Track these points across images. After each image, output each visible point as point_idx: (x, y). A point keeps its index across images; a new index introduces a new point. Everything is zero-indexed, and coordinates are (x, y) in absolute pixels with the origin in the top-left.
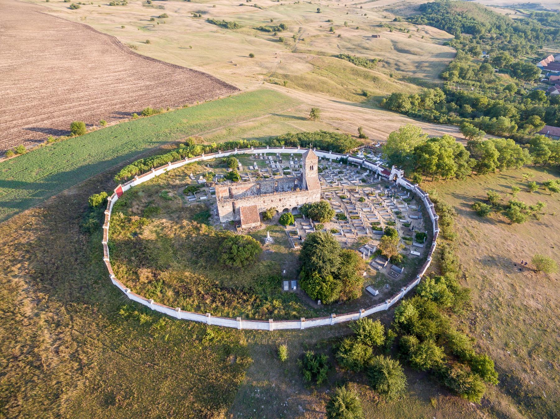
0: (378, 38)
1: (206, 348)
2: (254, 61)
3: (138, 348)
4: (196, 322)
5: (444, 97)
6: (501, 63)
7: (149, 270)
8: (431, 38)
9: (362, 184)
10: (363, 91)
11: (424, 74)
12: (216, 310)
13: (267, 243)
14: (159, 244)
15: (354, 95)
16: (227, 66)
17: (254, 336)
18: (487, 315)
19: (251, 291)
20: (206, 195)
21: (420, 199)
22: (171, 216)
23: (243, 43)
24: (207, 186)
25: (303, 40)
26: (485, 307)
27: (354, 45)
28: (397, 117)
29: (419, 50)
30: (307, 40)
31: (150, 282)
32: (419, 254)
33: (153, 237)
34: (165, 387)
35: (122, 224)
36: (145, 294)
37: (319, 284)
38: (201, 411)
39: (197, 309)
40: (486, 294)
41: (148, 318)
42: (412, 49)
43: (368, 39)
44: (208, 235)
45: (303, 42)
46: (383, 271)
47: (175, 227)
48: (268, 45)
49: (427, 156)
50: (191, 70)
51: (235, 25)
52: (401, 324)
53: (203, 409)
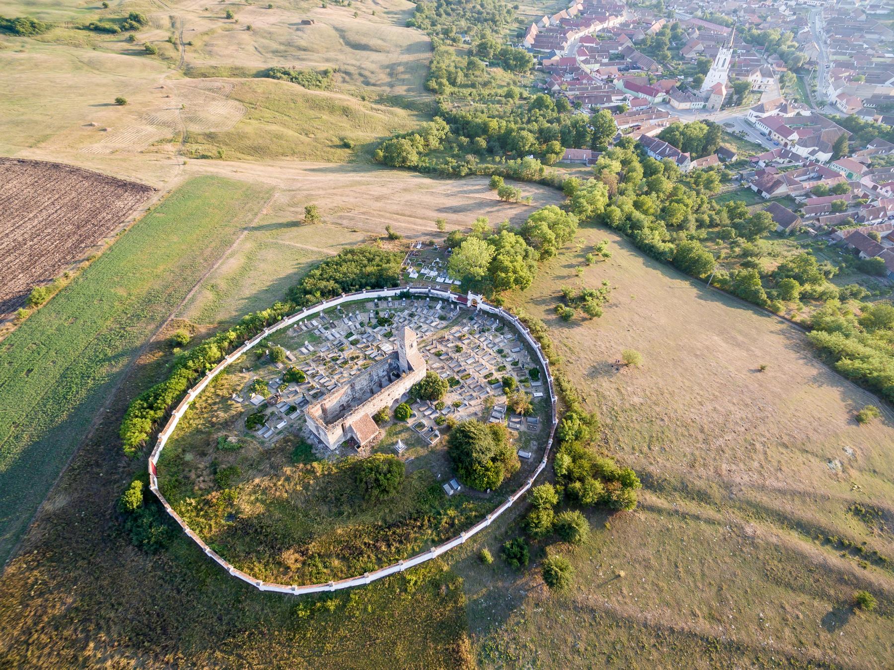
0: (313, 25)
1: (415, 594)
2: (130, 112)
3: (346, 637)
4: (389, 576)
5: (447, 127)
6: (488, 53)
7: (292, 551)
8: (385, 13)
9: (445, 323)
10: (342, 139)
11: (405, 88)
12: (398, 551)
13: (401, 451)
14: (277, 515)
15: (333, 150)
16: (90, 137)
17: (452, 556)
18: (612, 429)
19: (420, 514)
20: (281, 419)
21: (510, 323)
22: (260, 471)
23: (78, 68)
24: (272, 405)
25: (190, 44)
26: (608, 421)
27: (281, 44)
28: (405, 175)
29: (380, 42)
30: (198, 43)
31: (304, 563)
32: (541, 394)
33: (260, 509)
34: (400, 651)
35: (202, 513)
36: (310, 579)
37: (484, 475)
38: (447, 649)
39: (380, 564)
40: (604, 408)
41: (337, 602)
42: (373, 42)
43: (298, 30)
44: (329, 474)
45: (192, 48)
46: (523, 428)
47: (280, 483)
48: (131, 66)
49: (503, 275)
50: (22, 162)
51: (33, 25)
52: (564, 476)
53: (447, 646)
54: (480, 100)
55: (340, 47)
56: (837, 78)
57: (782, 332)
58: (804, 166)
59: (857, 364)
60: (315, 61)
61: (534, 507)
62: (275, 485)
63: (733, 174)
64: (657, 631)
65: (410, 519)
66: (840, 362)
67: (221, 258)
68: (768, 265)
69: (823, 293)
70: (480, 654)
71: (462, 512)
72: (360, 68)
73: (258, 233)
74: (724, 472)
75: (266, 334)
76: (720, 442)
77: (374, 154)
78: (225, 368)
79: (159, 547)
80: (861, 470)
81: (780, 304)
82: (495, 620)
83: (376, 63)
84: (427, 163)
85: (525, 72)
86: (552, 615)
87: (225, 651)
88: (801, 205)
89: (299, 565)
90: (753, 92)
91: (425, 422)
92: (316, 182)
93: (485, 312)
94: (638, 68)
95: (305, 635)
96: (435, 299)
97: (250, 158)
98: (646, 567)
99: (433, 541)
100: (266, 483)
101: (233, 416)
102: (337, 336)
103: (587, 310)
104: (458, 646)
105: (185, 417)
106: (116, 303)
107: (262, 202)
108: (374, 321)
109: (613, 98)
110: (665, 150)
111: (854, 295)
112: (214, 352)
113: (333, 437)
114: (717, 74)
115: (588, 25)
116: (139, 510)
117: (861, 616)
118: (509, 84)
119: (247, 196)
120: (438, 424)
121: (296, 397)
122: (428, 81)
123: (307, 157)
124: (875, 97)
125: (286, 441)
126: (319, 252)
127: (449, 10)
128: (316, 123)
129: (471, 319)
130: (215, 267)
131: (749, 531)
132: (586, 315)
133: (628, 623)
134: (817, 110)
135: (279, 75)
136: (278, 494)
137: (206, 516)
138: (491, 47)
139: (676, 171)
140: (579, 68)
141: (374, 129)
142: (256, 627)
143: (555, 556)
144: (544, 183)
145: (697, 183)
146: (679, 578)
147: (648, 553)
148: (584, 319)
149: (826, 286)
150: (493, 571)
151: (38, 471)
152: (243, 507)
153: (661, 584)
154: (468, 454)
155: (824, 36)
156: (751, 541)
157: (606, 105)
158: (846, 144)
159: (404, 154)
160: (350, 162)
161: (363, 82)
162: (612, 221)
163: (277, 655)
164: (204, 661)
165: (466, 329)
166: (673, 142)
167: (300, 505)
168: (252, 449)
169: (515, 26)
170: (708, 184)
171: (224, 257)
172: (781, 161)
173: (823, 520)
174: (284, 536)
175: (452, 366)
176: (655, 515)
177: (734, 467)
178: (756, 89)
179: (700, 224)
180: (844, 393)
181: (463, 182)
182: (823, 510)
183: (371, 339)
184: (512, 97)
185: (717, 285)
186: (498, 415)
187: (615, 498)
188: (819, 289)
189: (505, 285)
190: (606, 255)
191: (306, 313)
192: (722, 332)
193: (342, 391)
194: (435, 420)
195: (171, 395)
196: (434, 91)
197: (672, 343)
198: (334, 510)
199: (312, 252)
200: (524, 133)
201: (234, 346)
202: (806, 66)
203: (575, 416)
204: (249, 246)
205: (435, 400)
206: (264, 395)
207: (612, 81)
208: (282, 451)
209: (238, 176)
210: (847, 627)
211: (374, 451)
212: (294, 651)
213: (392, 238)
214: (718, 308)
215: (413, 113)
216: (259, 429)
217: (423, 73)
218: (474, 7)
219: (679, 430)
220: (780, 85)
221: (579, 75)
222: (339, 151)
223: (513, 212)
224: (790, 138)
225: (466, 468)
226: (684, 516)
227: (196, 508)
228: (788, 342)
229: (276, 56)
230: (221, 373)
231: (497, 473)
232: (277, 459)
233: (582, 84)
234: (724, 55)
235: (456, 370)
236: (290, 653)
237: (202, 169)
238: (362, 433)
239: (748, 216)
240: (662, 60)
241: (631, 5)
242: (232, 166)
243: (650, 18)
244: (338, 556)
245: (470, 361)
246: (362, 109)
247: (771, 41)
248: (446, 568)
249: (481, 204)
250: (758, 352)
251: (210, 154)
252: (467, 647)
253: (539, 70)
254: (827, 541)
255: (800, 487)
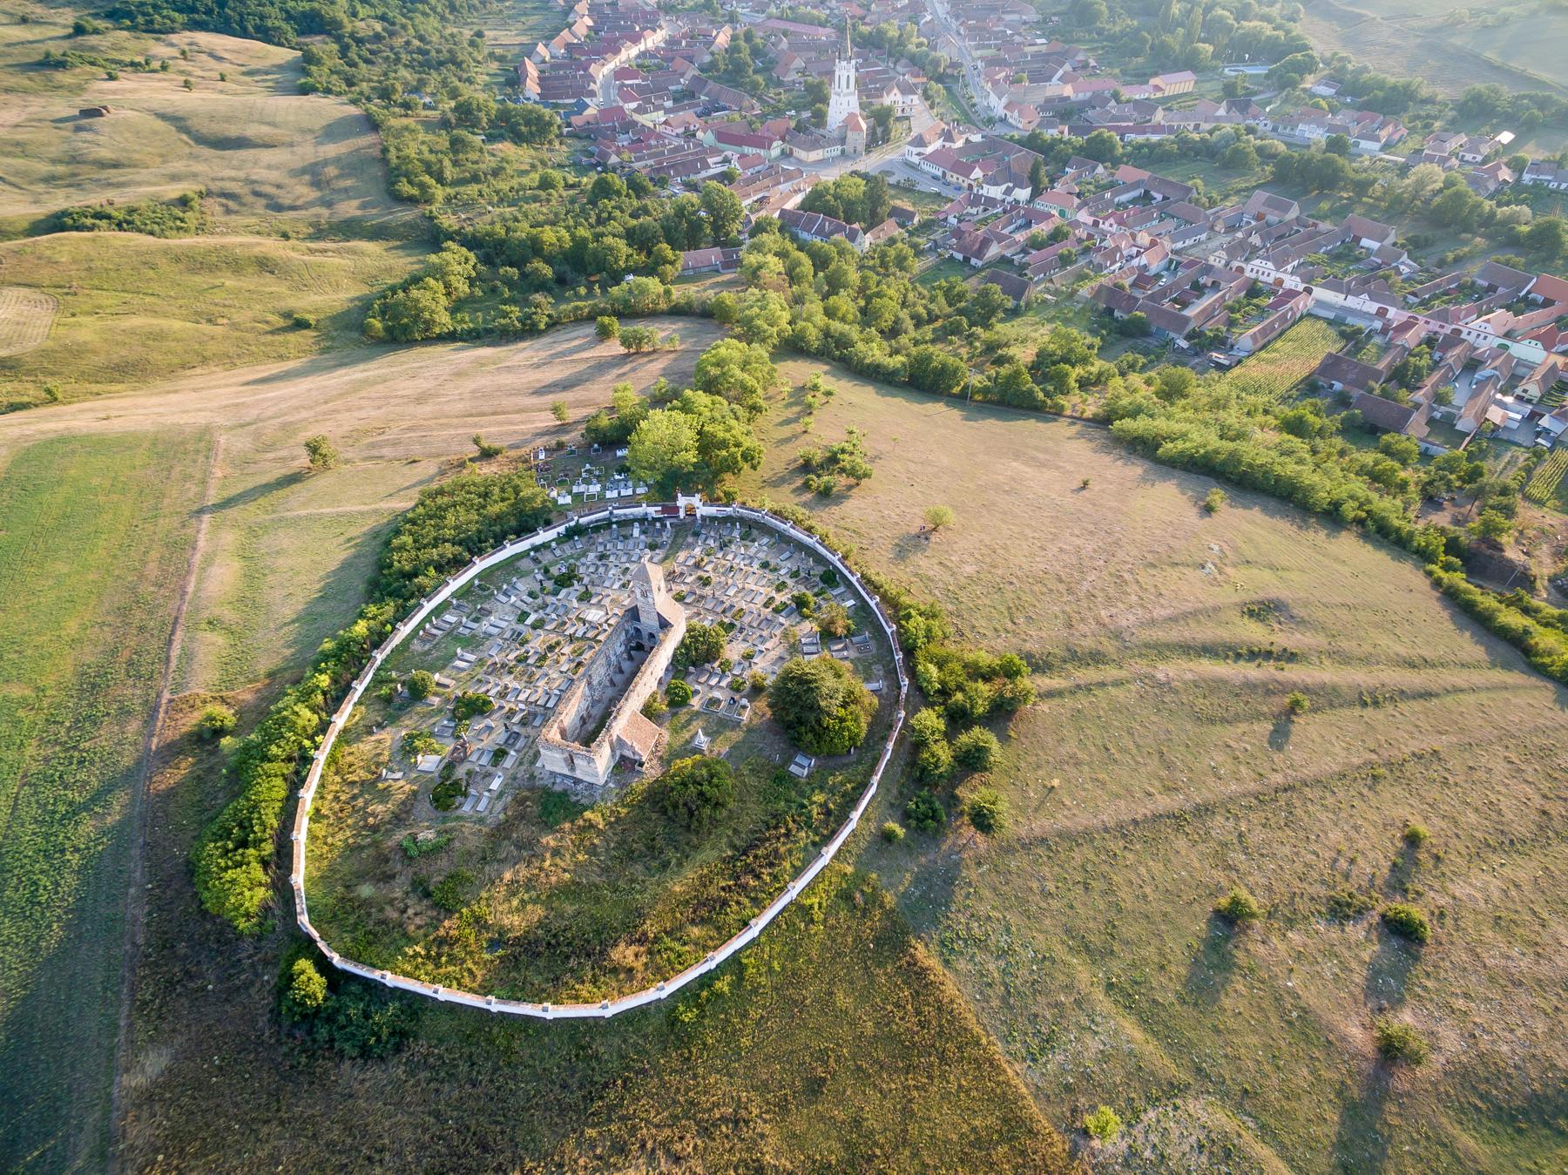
0: (108, 118)
1: (825, 920)
4: (780, 913)
5: (471, 255)
6: (479, 120)
7: (622, 946)
10: (287, 315)
11: (355, 203)
12: (775, 878)
13: (705, 747)
21: (756, 522)
24: (462, 760)
27: (54, 161)
29: (265, 129)
31: (650, 952)
32: (852, 602)
33: (537, 912)
35: (444, 959)
39: (759, 905)
43: (78, 129)
44: (618, 819)
49: (724, 453)
52: (938, 691)
54: (501, 200)
55: (187, 150)
56: (995, 83)
57: (1080, 435)
58: (1005, 212)
59: (1180, 445)
60: (150, 184)
61: (920, 745)
62: (541, 869)
63: (923, 242)
64: (1120, 831)
65: (768, 829)
66: (1160, 451)
67: (188, 572)
68: (1024, 355)
69: (1100, 374)
70: (942, 954)
71: (832, 791)
72: (249, 181)
73: (231, 513)
74: (1107, 620)
75: (378, 662)
76: (1086, 586)
77: (363, 329)
78: (339, 736)
79: (401, 1037)
80: (1235, 565)
81: (1061, 400)
82: (940, 905)
83: (278, 168)
84: (467, 322)
85: (550, 142)
86: (1001, 868)
87: (598, 1124)
88: (1024, 266)
89: (644, 959)
90: (898, 119)
91: (717, 694)
92: (283, 399)
93: (713, 519)
94: (724, 109)
95: (704, 1044)
96: (626, 523)
97: (119, 387)
98: (1076, 764)
99: (814, 844)
100: (524, 872)
101: (403, 803)
102: (503, 624)
103: (851, 472)
104: (912, 956)
105: (313, 838)
106: (21, 713)
107: (201, 459)
108: (549, 585)
109: (710, 161)
110: (822, 226)
111: (1132, 367)
112: (307, 718)
113: (599, 765)
114: (844, 100)
115: (617, 51)
116: (329, 1003)
117: (1300, 723)
118: (533, 166)
119: (160, 455)
120: (737, 690)
121: (493, 736)
122: (394, 183)
123: (238, 362)
124: (1048, 100)
125: (521, 802)
126: (376, 511)
127: (365, 53)
128: (218, 297)
129: (697, 535)
130: (191, 589)
131: (1160, 676)
132: (852, 481)
133: (1087, 836)
134: (987, 131)
135: (89, 221)
136: (554, 879)
137: (452, 960)
138: (480, 110)
139: (853, 254)
140: (634, 123)
141: (337, 287)
142: (628, 1068)
143: (971, 794)
144: (678, 312)
145: (884, 264)
146: (1115, 761)
147: (1071, 747)
148: (850, 488)
149: (1097, 366)
150: (907, 847)
151: (65, 1038)
152: (506, 922)
153: (1100, 776)
154: (814, 708)
155: (954, 24)
156: (1166, 686)
157: (704, 174)
158: (1043, 170)
159: (427, 315)
160: (324, 351)
161: (267, 207)
162: (808, 343)
163: (678, 1089)
164: (572, 1152)
165: (697, 551)
166: (830, 212)
167: (597, 880)
168: (471, 837)
169: (494, 66)
170: (901, 262)
171: (196, 570)
172: (974, 211)
173: (1223, 634)
174: (598, 933)
175: (709, 606)
176: (1057, 701)
177: (1114, 611)
178: (899, 114)
179: (919, 322)
180: (1179, 485)
181: (546, 340)
182: (1220, 623)
183: (561, 611)
184: (553, 187)
185: (978, 397)
186: (813, 649)
187: (1009, 695)
188: (1094, 369)
189: (731, 467)
190: (829, 393)
191: (428, 606)
192: (1017, 456)
193: (579, 693)
194: (730, 686)
195: (269, 811)
196: (412, 201)
197: (972, 486)
198: (655, 864)
199: (362, 513)
200: (609, 240)
201: (335, 700)
202: (949, 71)
203: (913, 613)
204: (229, 538)
205: (715, 659)
206: (437, 752)
207: (694, 135)
208: (523, 818)
209: (116, 426)
210: (1293, 738)
211: (666, 762)
212: (701, 1071)
213: (487, 454)
214: (993, 426)
215: (391, 244)
216: (461, 805)
217: (377, 171)
218: (408, 43)
219: (1035, 588)
220: (928, 103)
221: (642, 138)
222: (294, 338)
223: (658, 365)
224: (973, 176)
225: (812, 730)
226: (1088, 689)
227: (428, 956)
228: (1092, 445)
229: (57, 187)
230: (335, 747)
231: (856, 720)
232: (523, 832)
233: (649, 147)
234: (846, 71)
235: (719, 610)
236: (695, 1077)
237: (29, 430)
238: (639, 742)
239: (969, 296)
240: (753, 90)
241: (668, 9)
242: (91, 410)
243: (705, 26)
244: (693, 922)
245: (731, 592)
246: (294, 254)
247: (891, 40)
248: (849, 869)
249: (602, 367)
250: (1070, 467)
251: (25, 399)
252: (924, 954)
253: (569, 135)
254: (1238, 656)
255: (1189, 607)
